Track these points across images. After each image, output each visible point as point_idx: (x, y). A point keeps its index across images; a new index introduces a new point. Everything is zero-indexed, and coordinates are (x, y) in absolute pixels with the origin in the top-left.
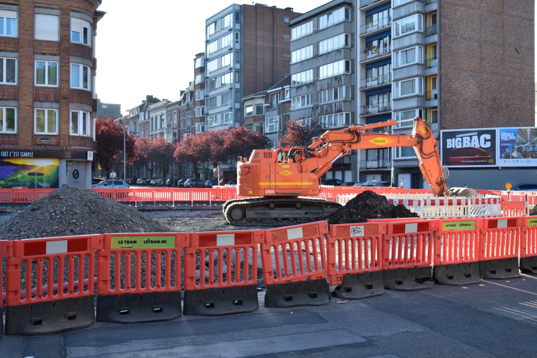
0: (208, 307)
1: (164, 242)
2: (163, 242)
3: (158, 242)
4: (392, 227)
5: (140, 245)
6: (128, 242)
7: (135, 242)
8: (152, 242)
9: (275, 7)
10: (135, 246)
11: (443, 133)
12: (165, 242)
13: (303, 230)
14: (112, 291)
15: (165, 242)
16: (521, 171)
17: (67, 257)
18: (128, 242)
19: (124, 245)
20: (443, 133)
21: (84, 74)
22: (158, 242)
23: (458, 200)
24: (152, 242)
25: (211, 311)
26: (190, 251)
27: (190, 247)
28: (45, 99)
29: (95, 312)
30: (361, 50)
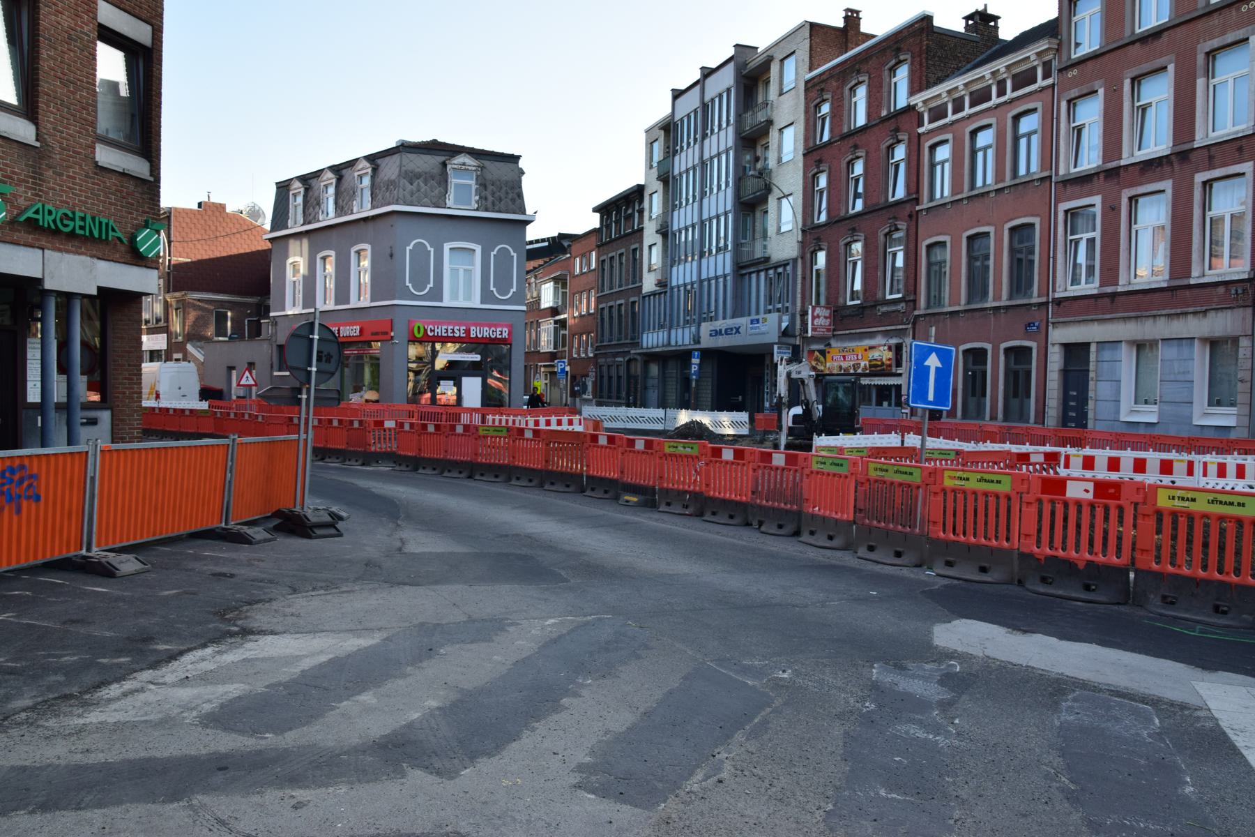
1: (999, 482)
2: (1239, 504)
3: (1231, 504)
5: (973, 484)
6: (1183, 499)
7: (1194, 500)
8: (1221, 503)
10: (1193, 507)
11: (1030, 349)
12: (1243, 505)
14: (1154, 566)
15: (1243, 505)
16: (1134, 297)
17: (1092, 505)
18: (1183, 499)
19: (1177, 503)
20: (1030, 349)
21: (477, 485)
22: (1231, 504)
23: (1162, 461)
24: (1221, 503)
26: (1026, 497)
27: (1144, 503)
28: (1213, 149)
29: (229, 324)
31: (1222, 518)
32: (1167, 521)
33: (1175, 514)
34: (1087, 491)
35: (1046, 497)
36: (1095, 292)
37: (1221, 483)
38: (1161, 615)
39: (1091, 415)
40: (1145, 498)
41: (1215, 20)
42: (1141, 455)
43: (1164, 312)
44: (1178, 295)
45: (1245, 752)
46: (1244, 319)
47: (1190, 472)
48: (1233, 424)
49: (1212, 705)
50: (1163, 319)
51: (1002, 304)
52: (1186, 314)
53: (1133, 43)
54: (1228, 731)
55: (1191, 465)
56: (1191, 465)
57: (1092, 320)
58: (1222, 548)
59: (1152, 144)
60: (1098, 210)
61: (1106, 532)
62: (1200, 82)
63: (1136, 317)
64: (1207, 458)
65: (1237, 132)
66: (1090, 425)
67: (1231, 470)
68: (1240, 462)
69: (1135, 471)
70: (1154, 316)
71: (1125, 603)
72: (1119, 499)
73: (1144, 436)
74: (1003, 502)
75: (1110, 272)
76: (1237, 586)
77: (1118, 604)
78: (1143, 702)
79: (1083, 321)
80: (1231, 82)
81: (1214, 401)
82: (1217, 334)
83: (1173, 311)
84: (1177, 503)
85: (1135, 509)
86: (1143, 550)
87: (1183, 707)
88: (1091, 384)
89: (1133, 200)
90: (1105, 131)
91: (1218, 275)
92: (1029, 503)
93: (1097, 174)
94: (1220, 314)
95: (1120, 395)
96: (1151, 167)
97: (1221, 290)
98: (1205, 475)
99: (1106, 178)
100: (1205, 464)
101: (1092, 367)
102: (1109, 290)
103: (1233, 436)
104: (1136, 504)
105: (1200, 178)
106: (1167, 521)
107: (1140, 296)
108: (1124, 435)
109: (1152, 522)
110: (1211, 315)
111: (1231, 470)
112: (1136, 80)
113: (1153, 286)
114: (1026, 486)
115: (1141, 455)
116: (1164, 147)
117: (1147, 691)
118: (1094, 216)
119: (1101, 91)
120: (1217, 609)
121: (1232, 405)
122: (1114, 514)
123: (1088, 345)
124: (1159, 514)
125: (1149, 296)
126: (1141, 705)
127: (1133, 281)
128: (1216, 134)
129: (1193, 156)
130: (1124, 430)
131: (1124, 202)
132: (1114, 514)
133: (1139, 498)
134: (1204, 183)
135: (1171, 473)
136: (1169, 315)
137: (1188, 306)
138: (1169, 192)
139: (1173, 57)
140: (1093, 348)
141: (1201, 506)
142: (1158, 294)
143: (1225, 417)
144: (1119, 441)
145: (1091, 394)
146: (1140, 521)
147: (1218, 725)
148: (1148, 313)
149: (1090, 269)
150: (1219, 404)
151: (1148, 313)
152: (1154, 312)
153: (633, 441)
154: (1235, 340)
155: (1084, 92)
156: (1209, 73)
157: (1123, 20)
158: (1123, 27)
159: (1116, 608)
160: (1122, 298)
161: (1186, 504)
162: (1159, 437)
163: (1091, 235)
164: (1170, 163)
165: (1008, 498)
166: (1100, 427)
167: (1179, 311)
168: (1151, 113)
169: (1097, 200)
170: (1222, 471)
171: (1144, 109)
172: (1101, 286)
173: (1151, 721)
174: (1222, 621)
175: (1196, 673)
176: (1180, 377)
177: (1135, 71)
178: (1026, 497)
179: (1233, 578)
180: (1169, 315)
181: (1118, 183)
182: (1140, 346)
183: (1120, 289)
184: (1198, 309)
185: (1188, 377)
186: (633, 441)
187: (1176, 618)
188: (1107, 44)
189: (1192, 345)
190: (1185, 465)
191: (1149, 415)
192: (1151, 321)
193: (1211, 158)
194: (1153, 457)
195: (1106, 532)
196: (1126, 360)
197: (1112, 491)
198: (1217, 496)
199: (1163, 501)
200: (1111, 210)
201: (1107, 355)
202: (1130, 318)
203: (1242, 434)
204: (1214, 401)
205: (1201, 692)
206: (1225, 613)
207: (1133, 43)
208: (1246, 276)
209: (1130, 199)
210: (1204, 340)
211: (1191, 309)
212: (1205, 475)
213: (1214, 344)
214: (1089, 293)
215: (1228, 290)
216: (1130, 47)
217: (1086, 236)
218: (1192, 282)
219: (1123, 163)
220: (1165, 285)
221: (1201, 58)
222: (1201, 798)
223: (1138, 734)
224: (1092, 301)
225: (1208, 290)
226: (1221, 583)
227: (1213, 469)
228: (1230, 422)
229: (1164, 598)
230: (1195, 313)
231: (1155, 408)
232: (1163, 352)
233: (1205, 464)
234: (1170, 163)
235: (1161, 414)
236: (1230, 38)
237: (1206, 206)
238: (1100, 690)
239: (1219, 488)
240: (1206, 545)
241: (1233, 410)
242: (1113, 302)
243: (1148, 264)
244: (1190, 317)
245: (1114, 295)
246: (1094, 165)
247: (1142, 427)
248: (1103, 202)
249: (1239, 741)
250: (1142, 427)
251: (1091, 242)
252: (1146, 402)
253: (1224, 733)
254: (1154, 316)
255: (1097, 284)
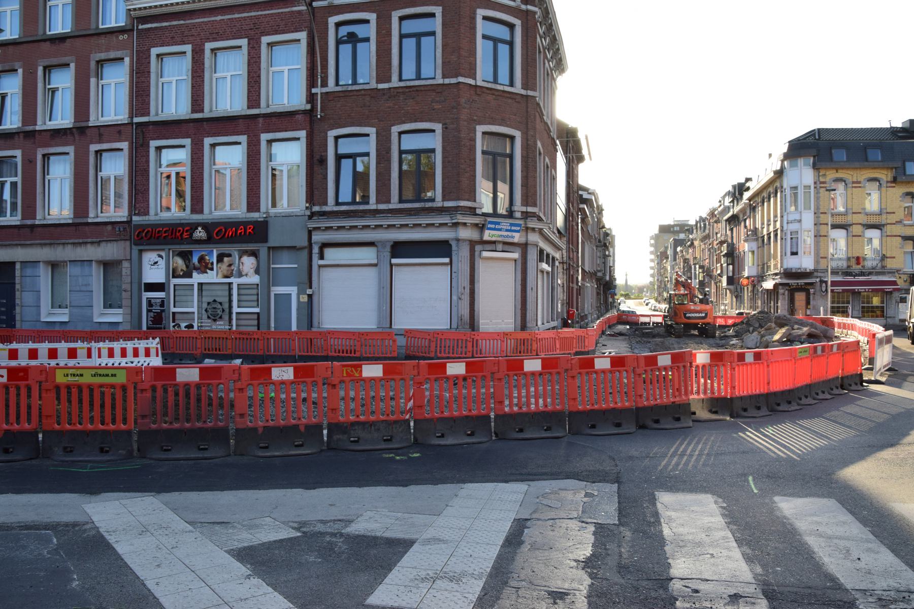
0: (469, 435)
2: (112, 375)
3: (107, 375)
4: (505, 364)
6: (74, 375)
7: (82, 375)
9: (560, 65)
12: (115, 375)
13: (466, 366)
14: (57, 426)
15: (115, 375)
18: (74, 375)
19: (70, 378)
22: (107, 375)
23: (69, 349)
25: (521, 436)
26: (140, 386)
27: (46, 381)
28: (102, 129)
30: (282, 179)
31: (101, 386)
32: (64, 393)
33: (68, 387)
34: (2, 376)
35: (159, 384)
36: (18, 223)
37: (110, 362)
38: (63, 461)
39: (18, 318)
40: (46, 378)
41: (103, 40)
42: (72, 345)
43: (71, 241)
44: (80, 229)
45: (115, 546)
46: (125, 248)
47: (89, 356)
48: (121, 320)
49: (95, 519)
50: (70, 246)
51: (391, 206)
52: (86, 243)
53: (45, 41)
54: (105, 534)
55: (89, 351)
56: (89, 351)
57: (17, 245)
58: (113, 407)
59: (113, 113)
60: (19, 160)
61: (29, 407)
62: (93, 81)
63: (50, 244)
64: (101, 345)
65: (117, 120)
66: (18, 325)
67: (117, 352)
68: (124, 346)
69: (30, 358)
70: (64, 244)
71: (36, 458)
72: (27, 379)
73: (59, 332)
74: (119, 394)
75: (29, 209)
76: (114, 432)
77: (31, 459)
78: (45, 529)
79: (9, 245)
80: (174, 82)
81: (108, 305)
82: (108, 258)
83: (76, 241)
84: (70, 378)
85: (40, 386)
86: (47, 416)
87: (75, 525)
88: (18, 294)
89: (46, 157)
90: (23, 102)
91: (107, 217)
92: (142, 391)
93: (18, 133)
94: (109, 244)
95: (40, 301)
96: (58, 135)
97: (109, 228)
98: (100, 357)
99: (25, 137)
100: (99, 349)
101: (17, 280)
102: (29, 222)
103: (121, 328)
104: (40, 382)
105: (94, 148)
106: (64, 393)
107: (52, 229)
108: (43, 332)
109: (53, 395)
110: (103, 244)
111: (117, 352)
112: (47, 69)
113: (62, 222)
114: (44, 376)
115: (72, 345)
116: (68, 122)
117: (48, 520)
118: (16, 165)
119: (20, 71)
120: (102, 450)
121: (120, 307)
122: (23, 392)
123: (14, 263)
124: (58, 387)
125: (59, 229)
126: (43, 532)
127: (48, 217)
128: (104, 119)
129: (88, 132)
130: (45, 328)
131: (39, 158)
132: (23, 392)
133: (43, 378)
134: (97, 152)
135: (76, 357)
136: (74, 244)
137: (88, 238)
138: (72, 154)
139: (74, 58)
140: (18, 266)
141: (87, 379)
142: (65, 228)
143: (115, 316)
144: (39, 336)
145: (18, 301)
146: (44, 395)
147: (98, 532)
148: (59, 242)
149: (14, 206)
150: (111, 307)
151: (59, 242)
152: (63, 241)
153: (743, 354)
154: (119, 262)
155: (7, 68)
156: (99, 76)
157: (37, 22)
158: (37, 26)
159: (29, 462)
160: (40, 229)
161: (77, 378)
162: (69, 332)
163: (14, 179)
164: (72, 134)
165: (124, 387)
166: (26, 326)
167: (81, 241)
168: (59, 95)
169: (18, 153)
170: (111, 354)
171: (54, 91)
172: (23, 219)
173: (51, 541)
174: (106, 457)
175: (87, 498)
176: (84, 288)
177: (47, 62)
178: (140, 386)
179: (112, 427)
180: (74, 244)
181: (34, 143)
182: (55, 266)
183: (37, 222)
184: (94, 240)
185: (89, 288)
186: (655, 357)
187: (73, 461)
188: (25, 36)
189: (91, 266)
190: (85, 351)
191: (62, 316)
192: (61, 247)
193: (100, 135)
194: (63, 347)
195: (29, 407)
196: (44, 277)
197: (21, 374)
198: (98, 371)
199: (60, 378)
200: (29, 163)
201: (29, 271)
202: (45, 244)
203: (126, 327)
204: (108, 305)
205: (88, 511)
206: (107, 452)
207: (45, 41)
208: (125, 219)
209: (44, 156)
210: (99, 262)
211: (89, 240)
212: (100, 357)
213: (108, 266)
214: (14, 224)
215: (114, 228)
216: (43, 43)
217: (10, 180)
218: (90, 221)
219: (38, 128)
220: (70, 221)
221: (93, 64)
222: (83, 587)
223: (40, 554)
224: (16, 230)
225: (101, 227)
226: (104, 431)
227: (105, 352)
228: (119, 319)
229: (65, 448)
230: (92, 243)
231: (66, 311)
232: (71, 270)
233: (99, 349)
234: (72, 134)
235: (71, 315)
236: (112, 55)
237: (98, 168)
238: (13, 528)
239: (110, 365)
240: (102, 406)
241: (120, 311)
242: (32, 231)
243: (59, 206)
244: (89, 246)
245: (33, 227)
246: (15, 126)
247: (58, 325)
248: (23, 155)
249: (111, 539)
250: (58, 325)
251: (14, 185)
252: (60, 307)
253: (102, 536)
254: (64, 244)
255: (19, 217)
